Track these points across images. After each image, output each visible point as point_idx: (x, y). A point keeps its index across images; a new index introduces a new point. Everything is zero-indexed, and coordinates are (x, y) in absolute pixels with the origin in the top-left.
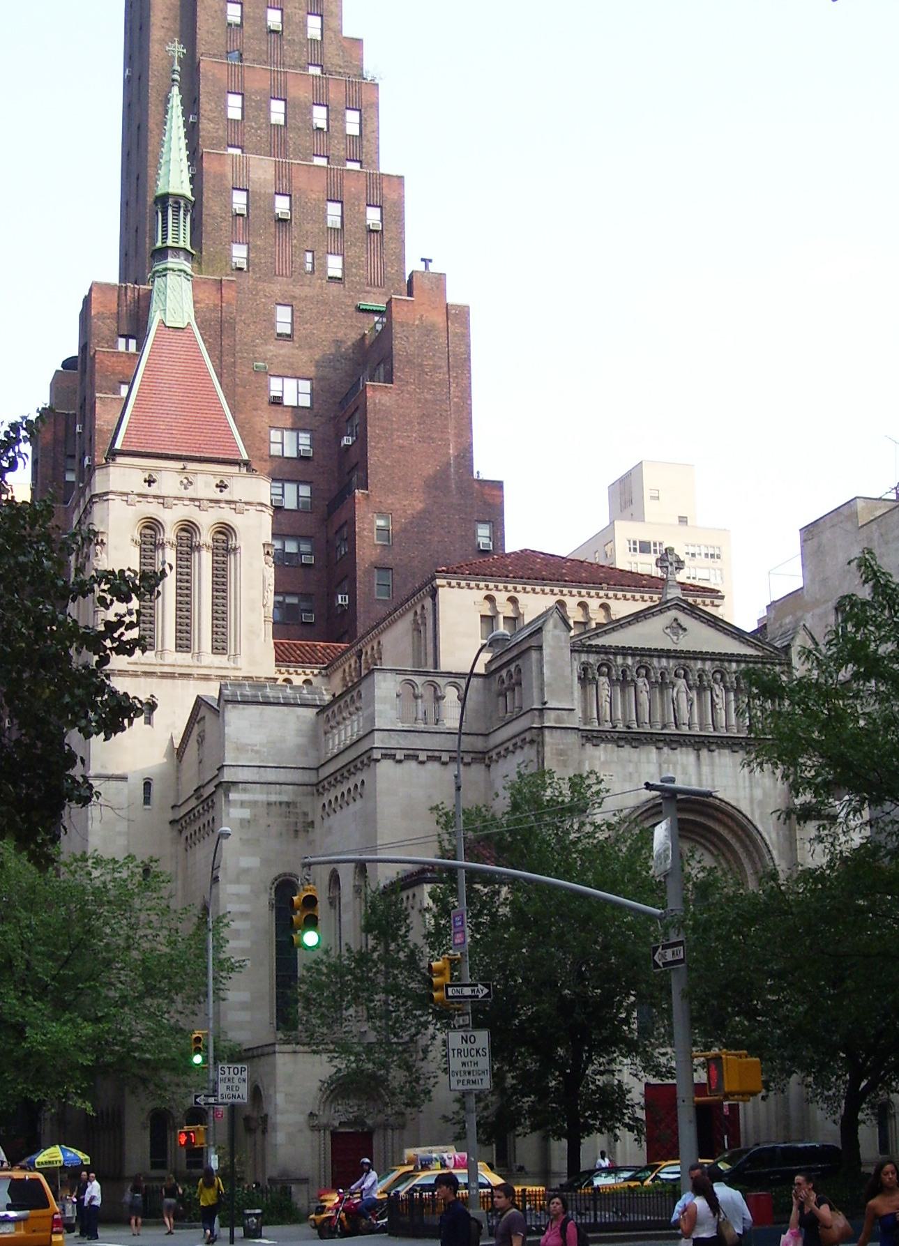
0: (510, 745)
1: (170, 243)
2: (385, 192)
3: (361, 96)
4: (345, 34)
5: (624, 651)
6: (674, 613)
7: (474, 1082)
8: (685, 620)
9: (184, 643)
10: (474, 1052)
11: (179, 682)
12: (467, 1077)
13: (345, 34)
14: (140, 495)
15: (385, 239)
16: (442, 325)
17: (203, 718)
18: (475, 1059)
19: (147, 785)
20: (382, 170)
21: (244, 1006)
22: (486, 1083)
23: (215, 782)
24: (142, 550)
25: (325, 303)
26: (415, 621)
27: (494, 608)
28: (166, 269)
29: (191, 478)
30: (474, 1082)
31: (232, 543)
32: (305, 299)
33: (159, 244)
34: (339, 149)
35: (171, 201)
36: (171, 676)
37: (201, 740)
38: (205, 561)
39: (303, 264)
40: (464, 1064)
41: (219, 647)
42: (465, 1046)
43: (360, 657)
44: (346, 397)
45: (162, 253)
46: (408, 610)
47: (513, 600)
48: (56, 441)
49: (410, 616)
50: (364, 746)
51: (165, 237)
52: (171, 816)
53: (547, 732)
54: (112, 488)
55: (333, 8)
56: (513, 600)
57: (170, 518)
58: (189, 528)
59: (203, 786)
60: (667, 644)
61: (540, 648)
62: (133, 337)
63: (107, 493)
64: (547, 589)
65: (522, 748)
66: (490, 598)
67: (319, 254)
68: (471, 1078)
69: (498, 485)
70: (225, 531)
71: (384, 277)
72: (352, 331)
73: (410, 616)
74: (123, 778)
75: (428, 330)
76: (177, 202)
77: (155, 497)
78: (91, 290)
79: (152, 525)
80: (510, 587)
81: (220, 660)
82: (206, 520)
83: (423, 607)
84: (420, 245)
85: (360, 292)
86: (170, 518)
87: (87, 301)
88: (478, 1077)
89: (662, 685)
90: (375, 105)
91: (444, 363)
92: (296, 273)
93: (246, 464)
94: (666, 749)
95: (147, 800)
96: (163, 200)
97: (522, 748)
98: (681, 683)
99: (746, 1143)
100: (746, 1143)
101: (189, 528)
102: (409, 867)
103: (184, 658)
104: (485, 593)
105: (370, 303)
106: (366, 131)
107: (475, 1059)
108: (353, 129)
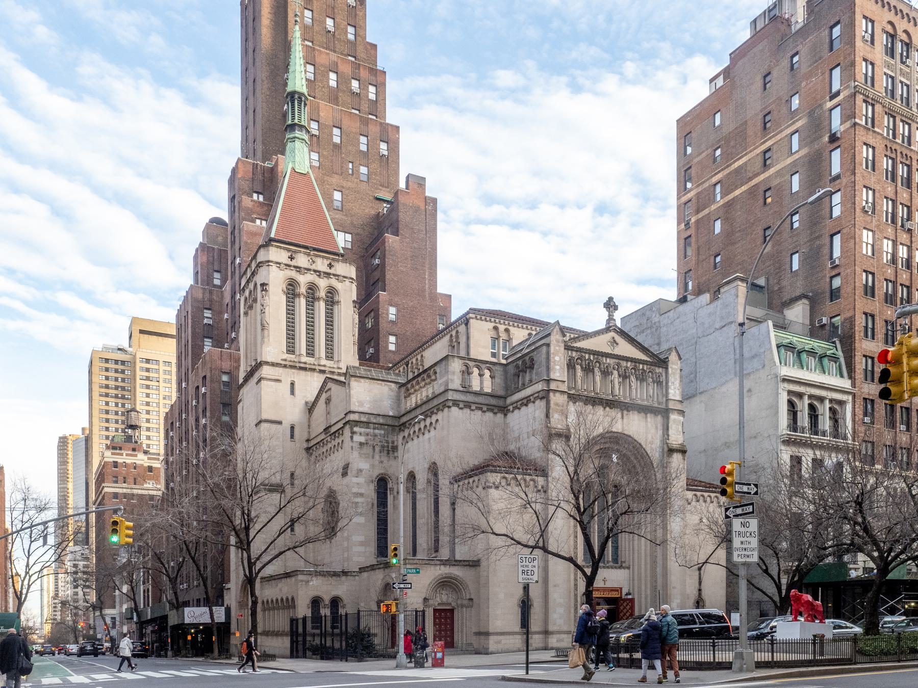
0: (525, 401)
1: (296, 121)
2: (390, 134)
3: (377, 77)
4: (368, 40)
5: (590, 352)
6: (612, 334)
7: (748, 556)
8: (618, 339)
9: (311, 353)
10: (748, 534)
11: (309, 373)
12: (744, 553)
13: (368, 40)
14: (286, 265)
15: (390, 162)
16: (423, 208)
17: (330, 389)
18: (749, 539)
19: (292, 428)
20: (387, 121)
21: (362, 544)
22: (755, 559)
23: (344, 421)
24: (288, 297)
25: (358, 192)
26: (451, 341)
27: (498, 333)
28: (295, 137)
29: (314, 258)
30: (748, 556)
31: (336, 299)
32: (349, 188)
33: (290, 122)
34: (365, 107)
35: (296, 96)
36: (305, 369)
37: (328, 401)
38: (321, 307)
39: (348, 168)
40: (742, 543)
41: (330, 356)
42: (743, 529)
43: (407, 365)
44: (371, 245)
45: (292, 127)
46: (445, 335)
47: (507, 330)
48: (208, 261)
49: (447, 338)
50: (441, 399)
51: (293, 118)
52: (305, 445)
53: (551, 394)
54: (271, 259)
55: (361, 23)
56: (507, 330)
57: (303, 280)
58: (312, 288)
59: (330, 426)
60: (608, 350)
61: (548, 345)
62: (261, 193)
63: (269, 261)
64: (525, 326)
65: (534, 402)
66: (496, 328)
67: (356, 164)
68: (746, 553)
69: (449, 297)
70: (332, 291)
71: (388, 183)
72: (370, 210)
73: (447, 338)
74: (280, 423)
75: (417, 210)
76: (300, 98)
77: (295, 267)
78: (237, 163)
79: (292, 285)
80: (507, 322)
81: (329, 363)
82: (323, 283)
83: (457, 332)
84: (409, 164)
85: (377, 189)
86: (303, 280)
87: (234, 171)
88: (750, 553)
89: (606, 373)
90: (384, 84)
91: (424, 228)
92: (343, 173)
93: (342, 256)
94: (608, 409)
95: (292, 436)
96: (292, 94)
97: (534, 402)
98: (615, 372)
99: (640, 610)
100: (640, 610)
101: (312, 288)
102: (258, 527)
103: (310, 360)
104: (493, 324)
105: (381, 195)
106: (380, 99)
107: (749, 539)
108: (372, 96)
